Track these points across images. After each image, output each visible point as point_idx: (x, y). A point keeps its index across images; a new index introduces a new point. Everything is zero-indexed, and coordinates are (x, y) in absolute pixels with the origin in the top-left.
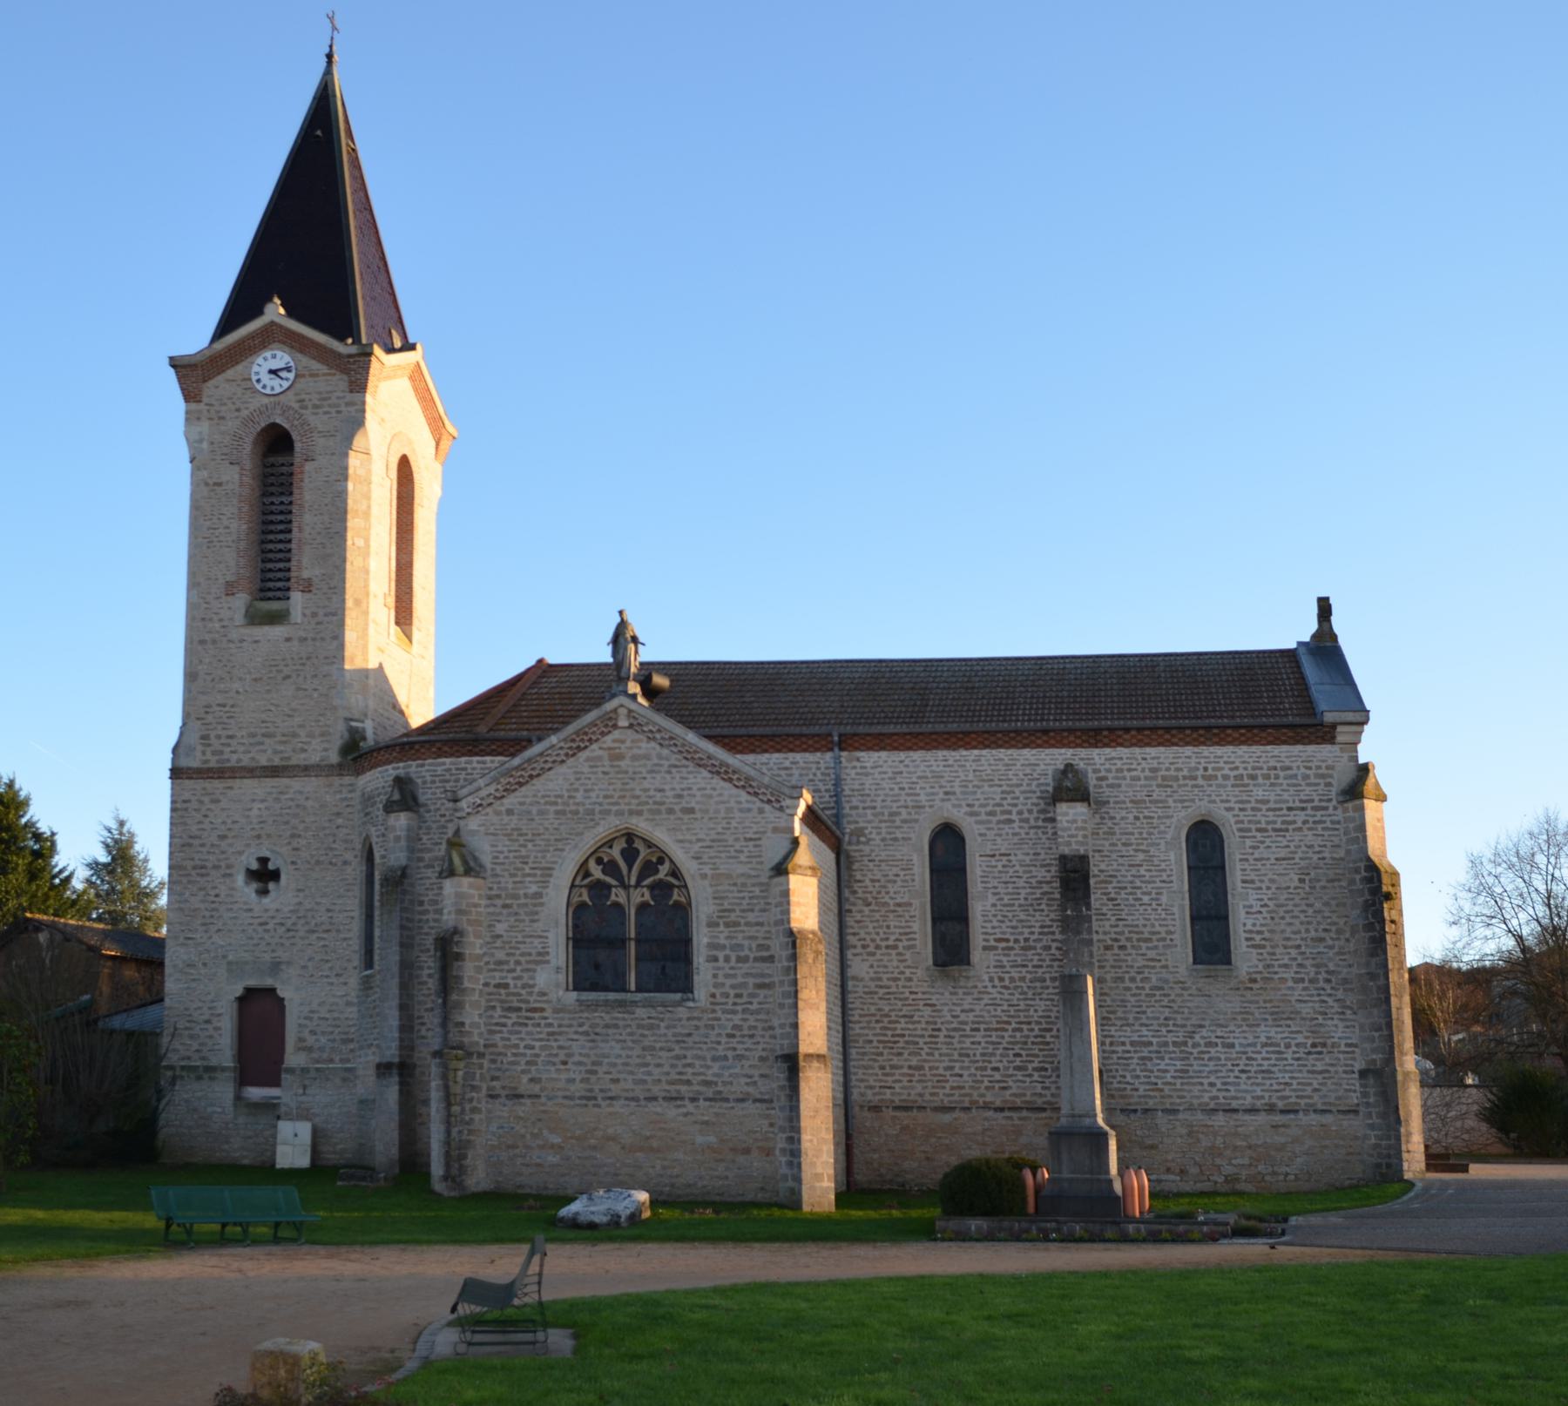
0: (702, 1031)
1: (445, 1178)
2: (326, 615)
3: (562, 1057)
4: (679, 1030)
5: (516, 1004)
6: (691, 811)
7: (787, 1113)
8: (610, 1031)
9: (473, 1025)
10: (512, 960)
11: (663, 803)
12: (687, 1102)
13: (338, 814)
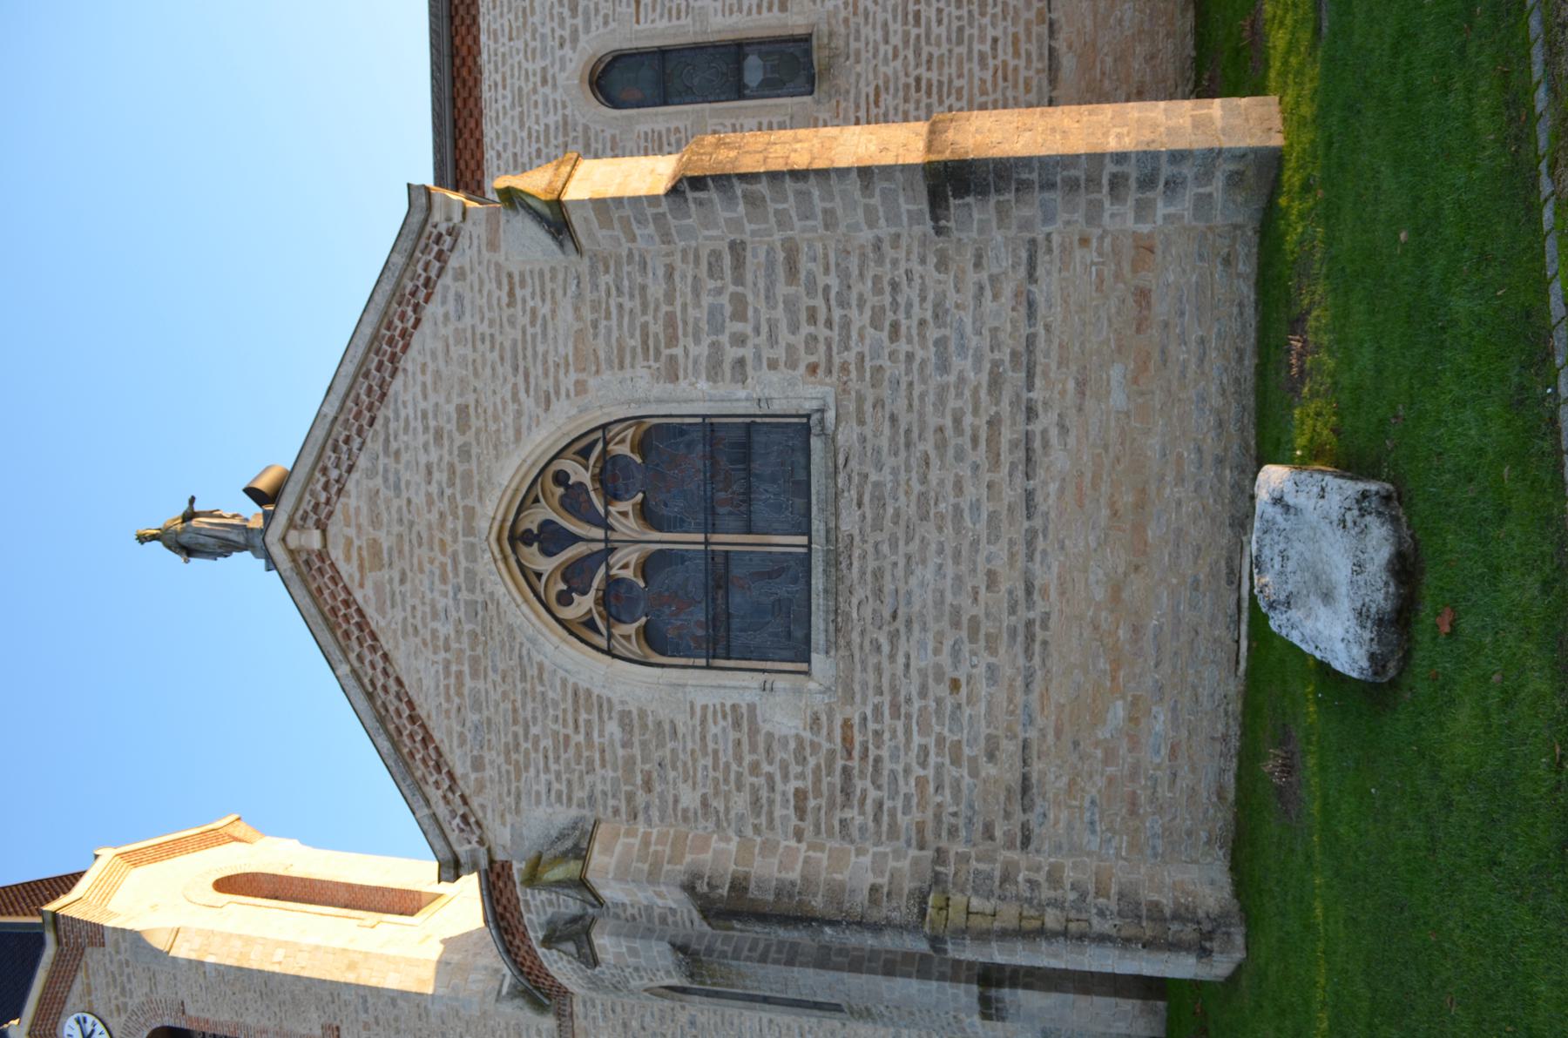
0: (886, 392)
1: (1204, 953)
2: (366, 1011)
3: (943, 690)
4: (884, 443)
5: (837, 779)
6: (462, 410)
7: (1056, 196)
8: (889, 587)
9: (877, 869)
10: (749, 780)
11: (452, 467)
12: (1036, 427)
13: (625, 1025)
